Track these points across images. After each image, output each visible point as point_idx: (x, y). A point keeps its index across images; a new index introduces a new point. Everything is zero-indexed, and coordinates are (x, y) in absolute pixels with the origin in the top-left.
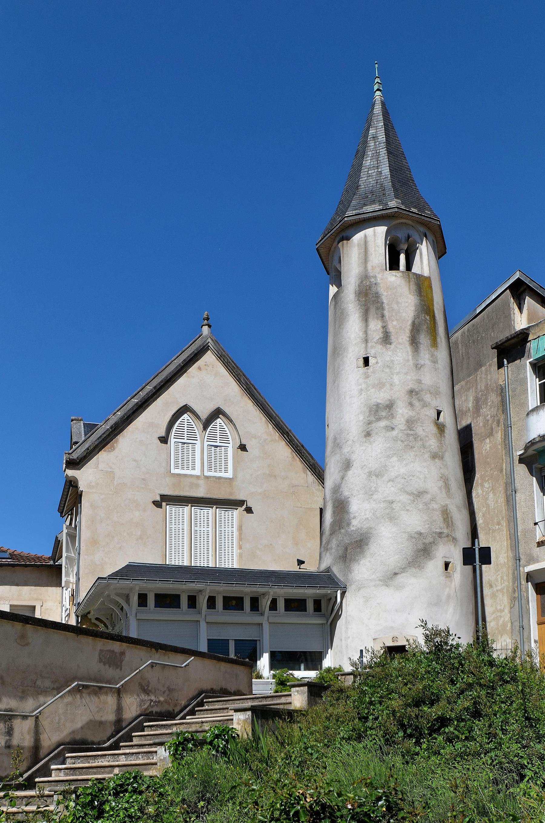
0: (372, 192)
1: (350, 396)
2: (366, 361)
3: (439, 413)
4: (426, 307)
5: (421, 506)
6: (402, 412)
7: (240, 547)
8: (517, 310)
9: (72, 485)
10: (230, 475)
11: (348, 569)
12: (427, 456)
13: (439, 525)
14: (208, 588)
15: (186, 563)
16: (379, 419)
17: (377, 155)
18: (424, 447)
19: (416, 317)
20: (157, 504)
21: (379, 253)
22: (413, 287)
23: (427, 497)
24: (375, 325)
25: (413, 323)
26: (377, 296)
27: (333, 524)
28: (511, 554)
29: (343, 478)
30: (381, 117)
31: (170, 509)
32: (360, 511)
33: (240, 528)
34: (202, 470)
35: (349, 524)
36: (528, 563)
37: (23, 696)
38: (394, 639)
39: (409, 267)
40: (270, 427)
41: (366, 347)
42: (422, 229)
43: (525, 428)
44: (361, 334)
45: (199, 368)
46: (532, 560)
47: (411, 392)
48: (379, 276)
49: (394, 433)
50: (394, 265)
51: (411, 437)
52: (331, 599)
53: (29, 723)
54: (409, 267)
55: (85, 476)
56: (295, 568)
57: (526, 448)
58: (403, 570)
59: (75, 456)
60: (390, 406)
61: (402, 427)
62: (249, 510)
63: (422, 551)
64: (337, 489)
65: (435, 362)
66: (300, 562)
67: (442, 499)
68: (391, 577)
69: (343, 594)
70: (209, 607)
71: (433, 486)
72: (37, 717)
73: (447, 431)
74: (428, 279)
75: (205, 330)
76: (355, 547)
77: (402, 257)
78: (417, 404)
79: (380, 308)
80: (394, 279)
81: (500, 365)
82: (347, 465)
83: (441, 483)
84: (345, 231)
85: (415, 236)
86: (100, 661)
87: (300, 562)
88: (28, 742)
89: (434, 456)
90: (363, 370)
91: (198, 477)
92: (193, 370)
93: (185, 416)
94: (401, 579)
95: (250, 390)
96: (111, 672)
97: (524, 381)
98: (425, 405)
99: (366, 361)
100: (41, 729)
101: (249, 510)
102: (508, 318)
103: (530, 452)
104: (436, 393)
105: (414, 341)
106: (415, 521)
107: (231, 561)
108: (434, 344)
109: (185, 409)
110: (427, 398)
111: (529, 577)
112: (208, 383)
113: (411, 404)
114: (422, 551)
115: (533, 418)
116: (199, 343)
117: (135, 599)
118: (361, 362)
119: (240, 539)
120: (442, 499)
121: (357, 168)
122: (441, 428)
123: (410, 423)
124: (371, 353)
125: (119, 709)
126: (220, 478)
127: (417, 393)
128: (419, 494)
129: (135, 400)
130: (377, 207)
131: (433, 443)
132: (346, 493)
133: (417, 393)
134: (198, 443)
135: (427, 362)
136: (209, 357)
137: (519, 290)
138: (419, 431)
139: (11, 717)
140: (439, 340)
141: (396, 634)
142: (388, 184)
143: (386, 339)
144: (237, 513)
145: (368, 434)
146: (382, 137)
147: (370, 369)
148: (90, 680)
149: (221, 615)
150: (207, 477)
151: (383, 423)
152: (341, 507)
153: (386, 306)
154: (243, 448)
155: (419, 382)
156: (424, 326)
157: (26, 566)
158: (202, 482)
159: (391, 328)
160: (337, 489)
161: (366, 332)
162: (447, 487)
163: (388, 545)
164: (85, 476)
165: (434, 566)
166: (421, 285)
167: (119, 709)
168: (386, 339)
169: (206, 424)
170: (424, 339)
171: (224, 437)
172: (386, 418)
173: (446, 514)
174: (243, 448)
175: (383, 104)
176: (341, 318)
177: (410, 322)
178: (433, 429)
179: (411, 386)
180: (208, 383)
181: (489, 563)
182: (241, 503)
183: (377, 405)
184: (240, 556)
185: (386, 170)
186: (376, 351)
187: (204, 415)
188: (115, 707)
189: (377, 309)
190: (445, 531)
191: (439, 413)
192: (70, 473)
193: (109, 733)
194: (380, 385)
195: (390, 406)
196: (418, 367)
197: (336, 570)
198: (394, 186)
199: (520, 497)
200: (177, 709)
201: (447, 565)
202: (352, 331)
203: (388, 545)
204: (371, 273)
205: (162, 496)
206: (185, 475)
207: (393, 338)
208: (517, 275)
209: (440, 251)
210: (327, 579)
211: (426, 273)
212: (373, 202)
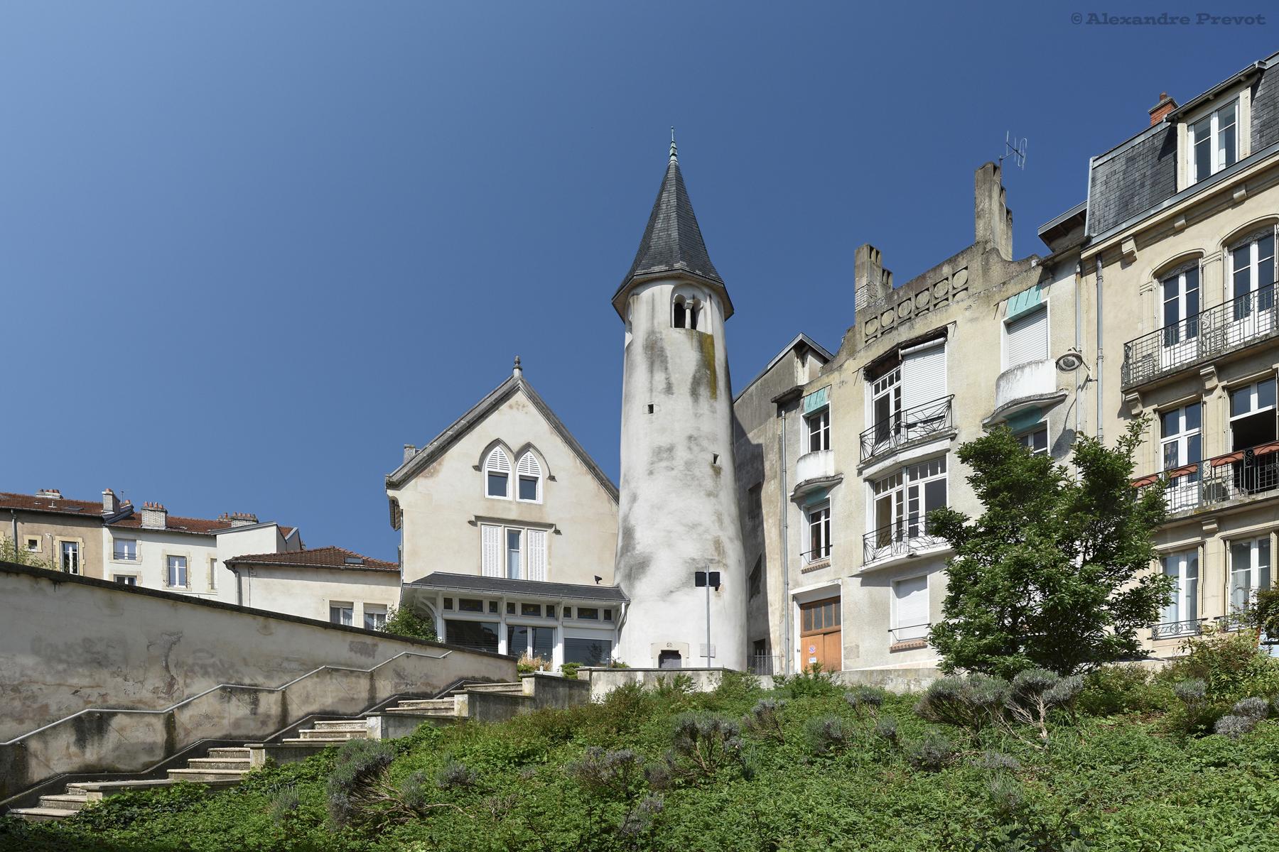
0: (661, 253)
1: (638, 438)
2: (651, 408)
3: (716, 457)
4: (707, 362)
5: (695, 536)
6: (682, 454)
9: (394, 503)
12: (702, 493)
13: (711, 553)
14: (508, 596)
15: (475, 573)
17: (668, 218)
20: (470, 522)
21: (665, 312)
22: (695, 343)
23: (701, 529)
24: (660, 377)
25: (694, 377)
26: (662, 350)
27: (623, 547)
28: (781, 579)
30: (674, 182)
31: (486, 529)
32: (644, 540)
33: (550, 547)
36: (794, 587)
37: (269, 676)
40: (578, 461)
42: (706, 291)
43: (795, 473)
44: (647, 384)
45: (511, 407)
46: (797, 584)
47: (690, 437)
49: (674, 473)
50: (679, 322)
51: (688, 476)
52: (618, 609)
53: (276, 697)
54: (694, 325)
55: (404, 497)
56: (593, 583)
57: (796, 491)
58: (678, 589)
59: (395, 479)
60: (671, 449)
61: (682, 468)
62: (557, 532)
64: (626, 519)
65: (714, 412)
66: (598, 579)
67: (715, 531)
70: (508, 612)
71: (707, 520)
72: (284, 693)
74: (711, 337)
75: (517, 372)
76: (636, 569)
77: (688, 313)
78: (695, 448)
79: (664, 360)
80: (679, 335)
81: (779, 415)
82: (634, 498)
83: (714, 518)
84: (631, 287)
85: (700, 295)
86: (351, 650)
87: (598, 579)
88: (275, 710)
89: (709, 494)
91: (510, 502)
93: (497, 449)
94: (675, 596)
95: (559, 428)
96: (363, 660)
97: (797, 432)
98: (703, 450)
99: (651, 408)
100: (289, 701)
101: (557, 532)
102: (791, 373)
103: (799, 494)
104: (714, 439)
105: (694, 393)
107: (542, 576)
108: (714, 394)
109: (496, 442)
110: (705, 443)
111: (795, 597)
112: (519, 420)
113: (690, 448)
115: (802, 464)
116: (510, 384)
117: (441, 603)
118: (647, 409)
119: (550, 556)
120: (715, 531)
121: (650, 228)
122: (717, 471)
123: (689, 465)
125: (373, 689)
128: (694, 526)
129: (450, 433)
130: (663, 268)
131: (709, 483)
132: (633, 522)
135: (707, 412)
136: (520, 397)
137: (802, 350)
138: (697, 472)
139: (256, 691)
142: (676, 248)
143: (669, 389)
144: (546, 534)
145: (651, 473)
146: (673, 202)
148: (341, 664)
149: (575, 621)
151: (664, 464)
152: (628, 533)
154: (552, 478)
155: (699, 429)
156: (705, 378)
157: (353, 570)
158: (514, 507)
159: (673, 380)
160: (626, 519)
162: (720, 520)
164: (404, 497)
166: (705, 343)
167: (373, 689)
168: (669, 389)
169: (518, 455)
170: (704, 391)
172: (667, 459)
173: (718, 544)
174: (552, 478)
175: (677, 168)
176: (632, 367)
177: (691, 376)
178: (709, 471)
179: (690, 432)
180: (519, 420)
181: (863, 584)
182: (551, 526)
183: (660, 448)
184: (550, 571)
185: (675, 234)
186: (659, 400)
187: (516, 448)
188: (368, 687)
191: (716, 457)
192: (391, 493)
193: (362, 706)
195: (671, 449)
197: (623, 587)
198: (681, 248)
200: (437, 691)
202: (639, 382)
203: (668, 566)
205: (477, 517)
207: (675, 389)
208: (800, 337)
209: (728, 310)
210: (616, 593)
211: (709, 332)
212: (660, 263)
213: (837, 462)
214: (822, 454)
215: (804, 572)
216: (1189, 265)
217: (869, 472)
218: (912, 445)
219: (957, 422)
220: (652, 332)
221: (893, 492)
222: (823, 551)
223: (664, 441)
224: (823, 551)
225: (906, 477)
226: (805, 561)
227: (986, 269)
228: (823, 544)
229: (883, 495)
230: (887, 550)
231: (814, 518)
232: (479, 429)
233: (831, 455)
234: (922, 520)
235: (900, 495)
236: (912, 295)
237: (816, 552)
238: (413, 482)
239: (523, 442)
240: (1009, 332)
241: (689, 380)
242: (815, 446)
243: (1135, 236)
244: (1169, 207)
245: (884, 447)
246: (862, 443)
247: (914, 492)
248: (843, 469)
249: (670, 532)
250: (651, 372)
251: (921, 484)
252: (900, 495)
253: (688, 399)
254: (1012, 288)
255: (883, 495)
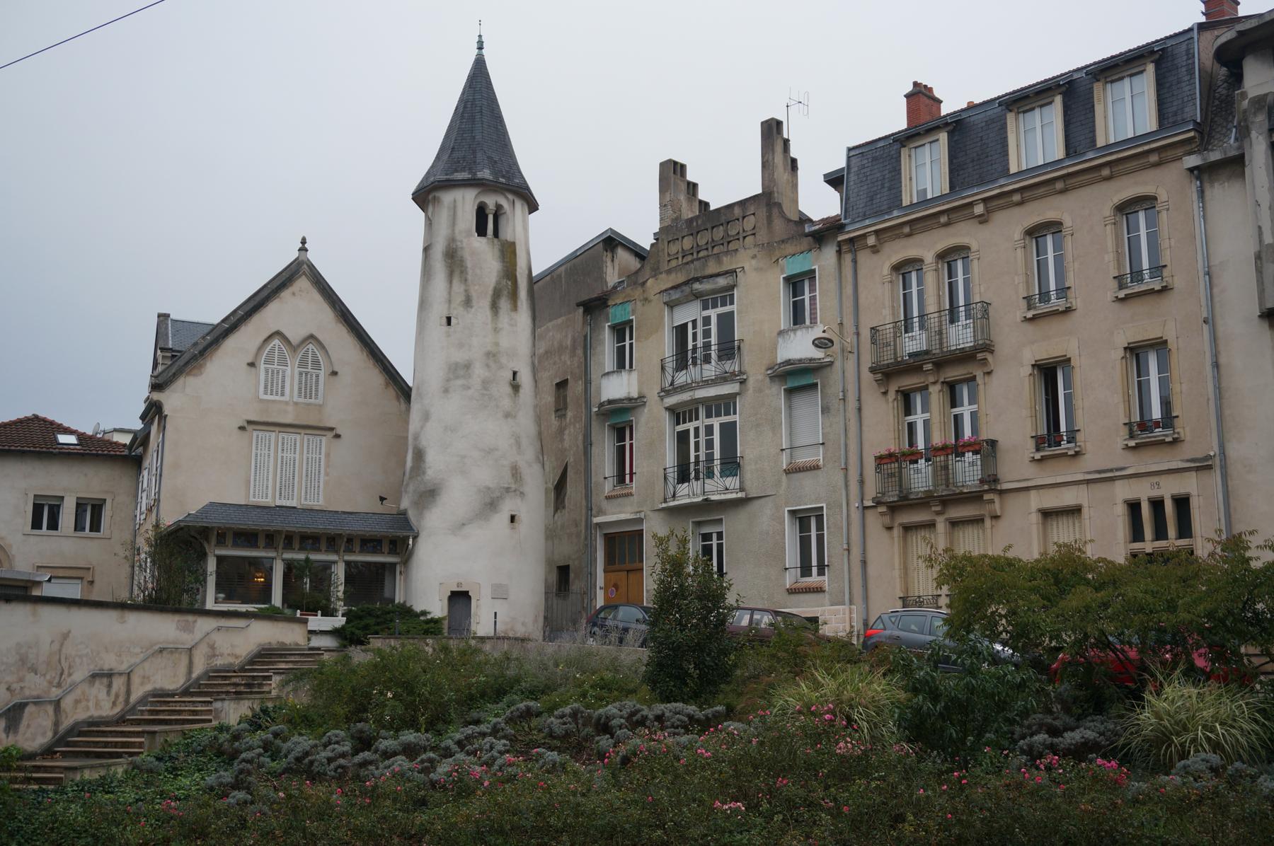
2: (449, 320)
3: (515, 373)
6: (479, 372)
7: (327, 474)
8: (609, 263)
10: (320, 401)
11: (420, 515)
13: (507, 480)
16: (457, 377)
18: (497, 406)
19: (498, 283)
20: (242, 428)
21: (468, 218)
22: (497, 253)
26: (462, 260)
27: (412, 468)
29: (422, 428)
33: (328, 455)
34: (291, 396)
35: (424, 473)
38: (459, 585)
39: (496, 234)
41: (449, 308)
46: (601, 512)
47: (489, 354)
48: (465, 241)
49: (470, 392)
50: (481, 231)
54: (496, 234)
56: (378, 508)
60: (468, 366)
62: (337, 436)
63: (490, 504)
66: (382, 499)
68: (460, 527)
69: (415, 538)
73: (521, 391)
76: (429, 495)
79: (463, 271)
80: (480, 244)
82: (426, 417)
87: (382, 499)
89: (507, 415)
90: (446, 328)
91: (287, 403)
92: (286, 294)
99: (449, 320)
105: (494, 307)
106: (485, 476)
108: (515, 307)
109: (278, 334)
110: (504, 360)
113: (487, 366)
114: (490, 504)
118: (445, 320)
119: (327, 466)
122: (516, 387)
123: (486, 384)
124: (453, 314)
126: (309, 404)
127: (494, 356)
128: (490, 451)
131: (506, 403)
133: (494, 356)
134: (289, 369)
140: (519, 304)
141: (461, 580)
143: (468, 302)
145: (446, 391)
147: (452, 328)
150: (296, 404)
151: (460, 382)
153: (470, 272)
155: (497, 344)
158: (290, 408)
159: (474, 295)
161: (450, 293)
162: (518, 444)
163: (457, 498)
165: (502, 518)
168: (468, 302)
170: (504, 304)
171: (316, 363)
173: (515, 472)
178: (508, 390)
182: (332, 429)
183: (457, 364)
186: (457, 312)
189: (462, 272)
190: (513, 486)
191: (515, 373)
194: (461, 345)
195: (468, 366)
196: (496, 330)
199: (595, 450)
201: (513, 519)
204: (458, 237)
205: (249, 422)
206: (274, 401)
207: (474, 303)
212: (463, 170)
213: (640, 383)
214: (624, 375)
215: (608, 498)
216: (913, 263)
217: (672, 400)
218: (707, 383)
219: (746, 367)
220: (452, 240)
221: (691, 426)
222: (628, 477)
223: (459, 356)
224: (628, 477)
225: (702, 413)
226: (608, 487)
227: (769, 219)
228: (627, 471)
229: (681, 428)
230: (683, 489)
231: (621, 438)
232: (257, 319)
233: (634, 375)
234: (717, 462)
235: (697, 429)
236: (709, 226)
237: (621, 478)
238: (180, 382)
239: (304, 333)
240: (159, 316)
241: (491, 292)
242: (621, 365)
243: (877, 232)
244: (896, 218)
245: (682, 378)
246: (663, 368)
247: (709, 430)
248: (646, 392)
249: (464, 457)
250: (451, 282)
251: (716, 423)
252: (697, 429)
253: (488, 313)
254: (790, 248)
255: (681, 428)
